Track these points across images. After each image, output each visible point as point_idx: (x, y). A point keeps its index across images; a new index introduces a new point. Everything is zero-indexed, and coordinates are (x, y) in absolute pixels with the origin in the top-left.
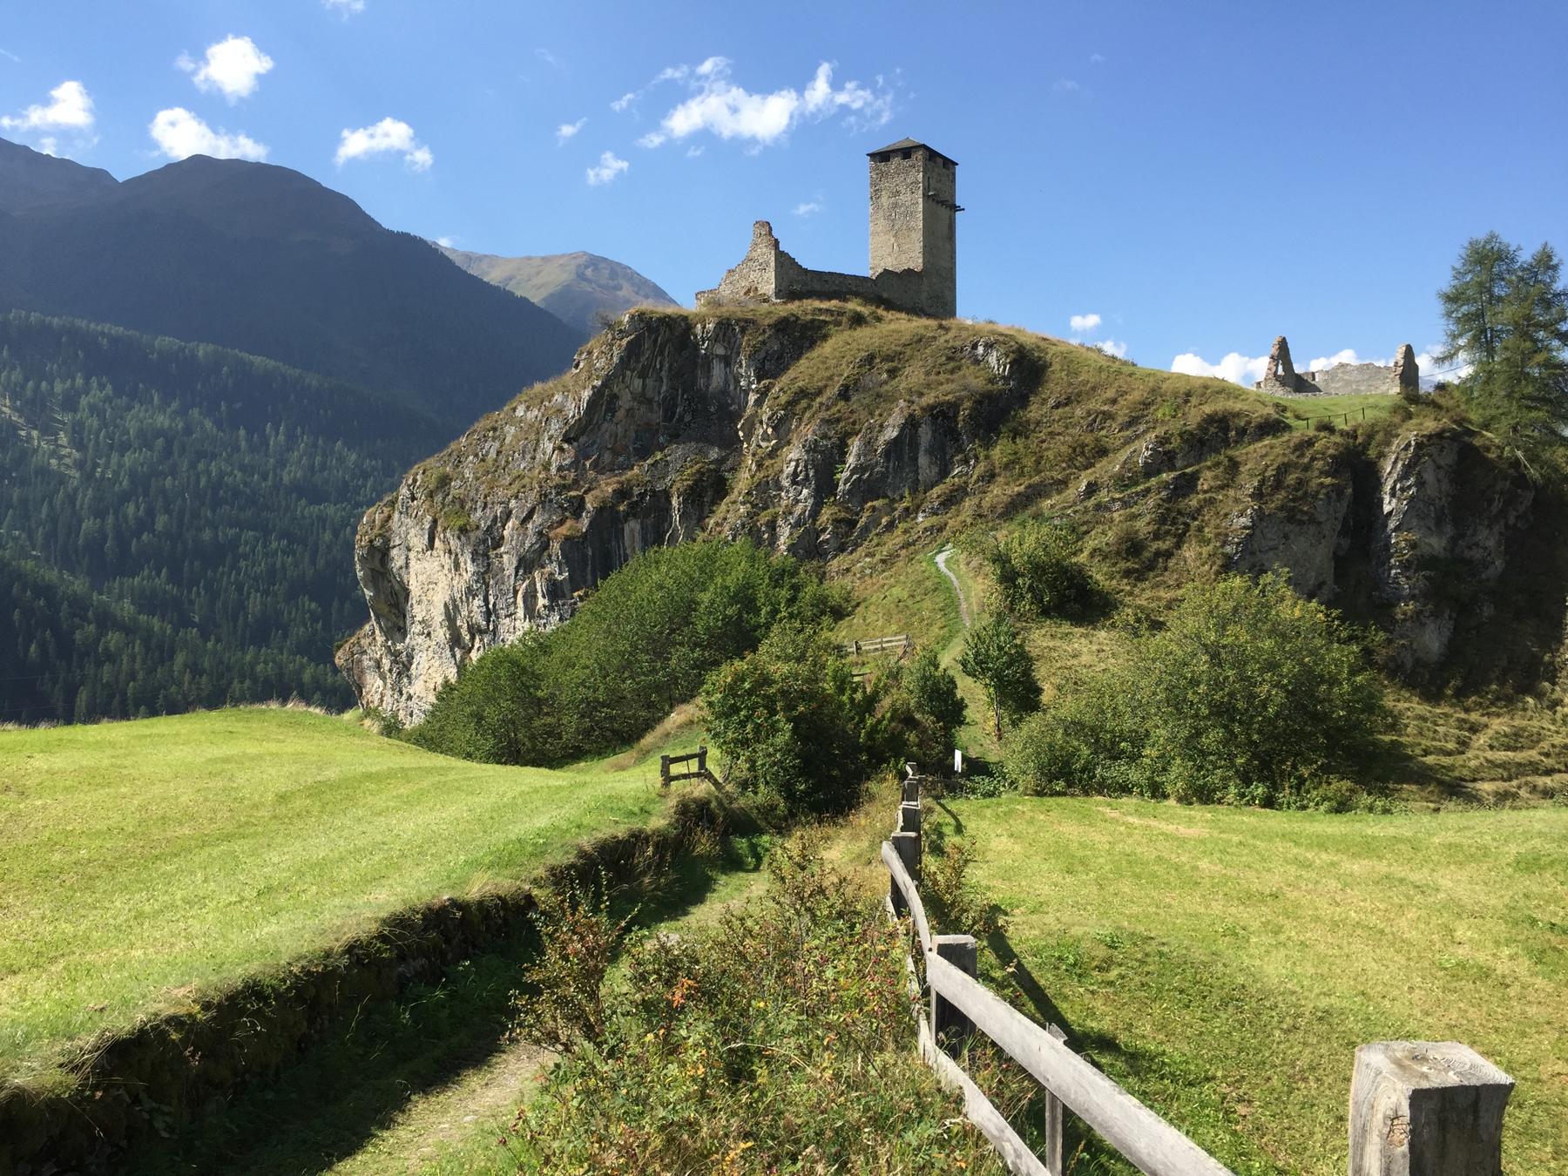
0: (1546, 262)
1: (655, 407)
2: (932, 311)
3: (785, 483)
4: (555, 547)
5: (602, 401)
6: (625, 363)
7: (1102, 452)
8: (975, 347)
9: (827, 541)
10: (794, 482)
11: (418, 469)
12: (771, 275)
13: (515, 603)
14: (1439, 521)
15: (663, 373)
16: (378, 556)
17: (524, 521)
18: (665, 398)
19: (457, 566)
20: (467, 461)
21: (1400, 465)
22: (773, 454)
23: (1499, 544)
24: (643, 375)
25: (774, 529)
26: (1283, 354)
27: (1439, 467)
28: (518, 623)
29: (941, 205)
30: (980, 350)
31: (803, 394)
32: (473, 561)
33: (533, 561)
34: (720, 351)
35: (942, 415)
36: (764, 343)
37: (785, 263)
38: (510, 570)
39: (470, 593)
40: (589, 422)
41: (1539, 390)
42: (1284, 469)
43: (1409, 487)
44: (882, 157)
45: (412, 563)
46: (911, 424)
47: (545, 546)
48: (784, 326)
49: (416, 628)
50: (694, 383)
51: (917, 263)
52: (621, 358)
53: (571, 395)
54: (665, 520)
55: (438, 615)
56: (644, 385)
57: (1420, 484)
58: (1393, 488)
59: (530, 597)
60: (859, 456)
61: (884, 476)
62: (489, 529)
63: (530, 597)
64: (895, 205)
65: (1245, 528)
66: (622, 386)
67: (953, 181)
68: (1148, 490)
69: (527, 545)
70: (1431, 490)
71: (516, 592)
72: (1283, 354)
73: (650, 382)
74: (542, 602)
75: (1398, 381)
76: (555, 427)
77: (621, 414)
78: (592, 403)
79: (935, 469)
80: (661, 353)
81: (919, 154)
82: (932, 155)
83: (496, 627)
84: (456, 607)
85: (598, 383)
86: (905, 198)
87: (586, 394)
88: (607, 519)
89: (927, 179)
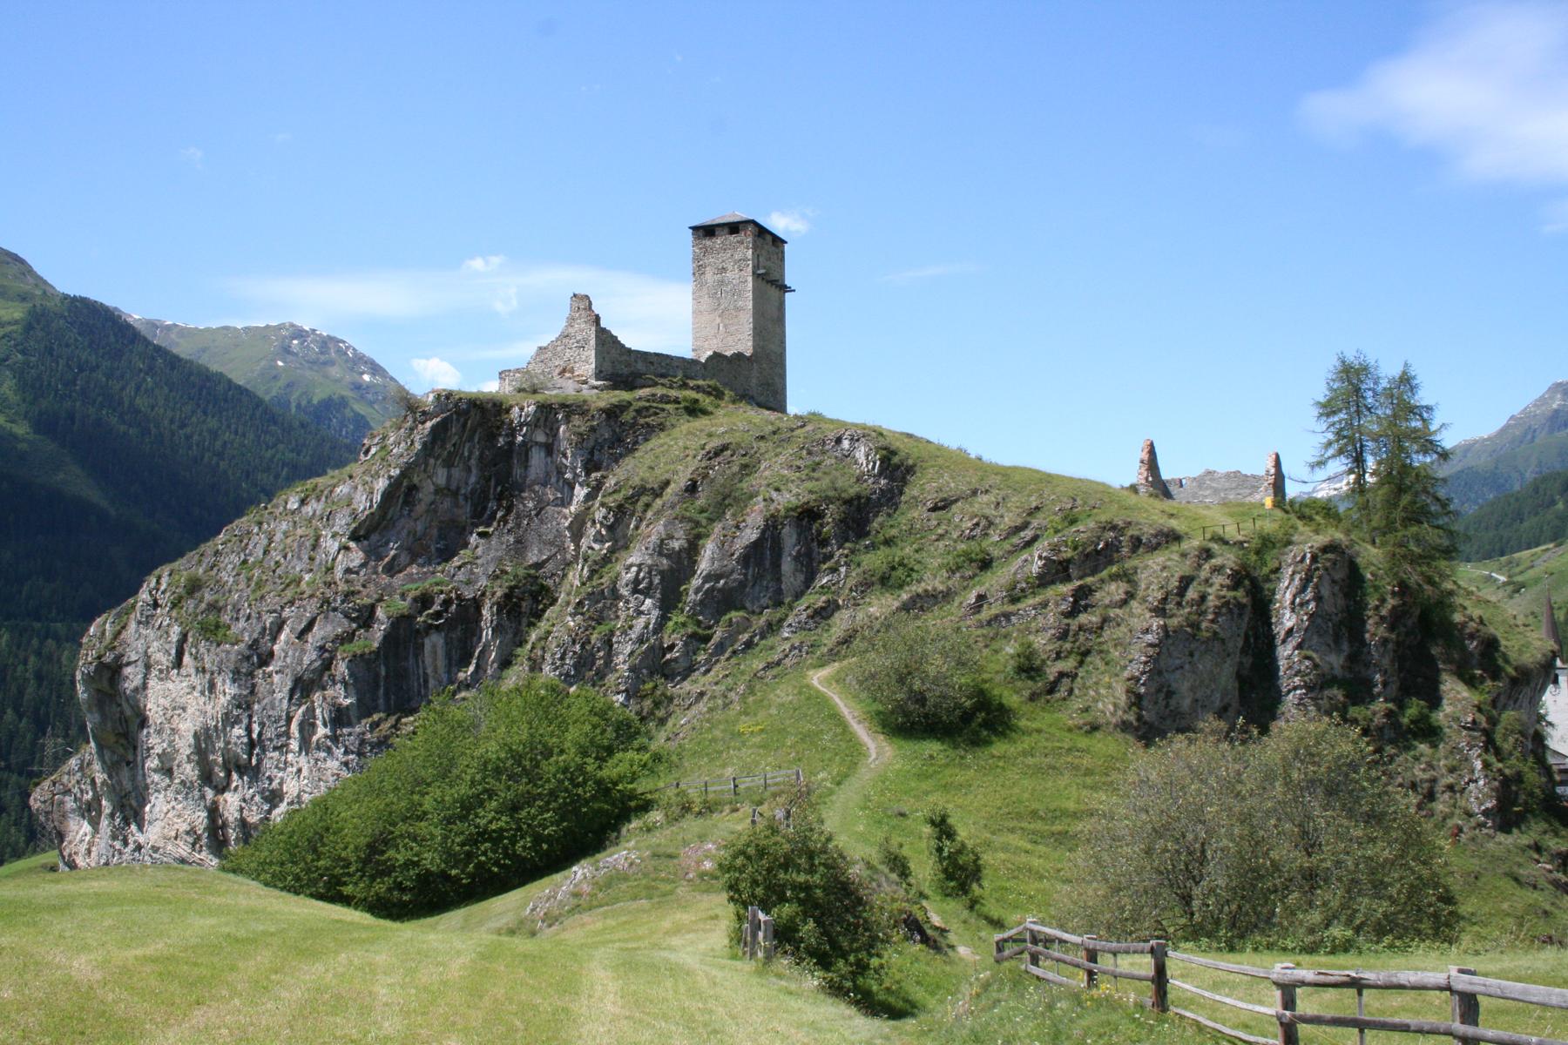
0: (1406, 380)
2: (762, 399)
3: (624, 592)
4: (341, 668)
5: (401, 493)
6: (430, 447)
7: (986, 564)
8: (839, 441)
9: (675, 660)
10: (635, 591)
11: (165, 571)
12: (590, 354)
13: (287, 734)
14: (1337, 639)
15: (473, 462)
16: (107, 674)
17: (302, 635)
18: (473, 492)
19: (212, 686)
20: (225, 559)
21: (1297, 577)
22: (606, 560)
23: (1392, 661)
24: (449, 464)
25: (611, 646)
26: (1152, 464)
27: (1334, 581)
28: (290, 756)
30: (846, 444)
32: (234, 681)
33: (312, 681)
34: (540, 437)
35: (808, 515)
37: (606, 341)
38: (282, 695)
39: (229, 720)
40: (383, 517)
42: (1186, 582)
43: (1308, 602)
44: (706, 232)
45: (151, 683)
46: (772, 527)
47: (327, 665)
48: (612, 413)
49: (153, 763)
50: (509, 474)
51: (746, 346)
52: (425, 445)
53: (360, 489)
54: (473, 635)
55: (185, 746)
56: (449, 477)
57: (1318, 598)
58: (1293, 603)
59: (307, 727)
60: (713, 560)
61: (742, 584)
62: (254, 645)
63: (307, 727)
64: (721, 283)
65: (1151, 645)
66: (423, 476)
68: (1045, 605)
69: (306, 661)
70: (1328, 607)
71: (289, 719)
72: (1152, 464)
73: (457, 473)
74: (322, 731)
75: (1271, 491)
76: (342, 522)
77: (420, 508)
78: (388, 495)
79: (801, 577)
80: (471, 439)
82: (762, 232)
83: (260, 761)
84: (208, 737)
85: (395, 472)
86: (732, 275)
87: (381, 484)
88: (403, 635)
89: (756, 256)
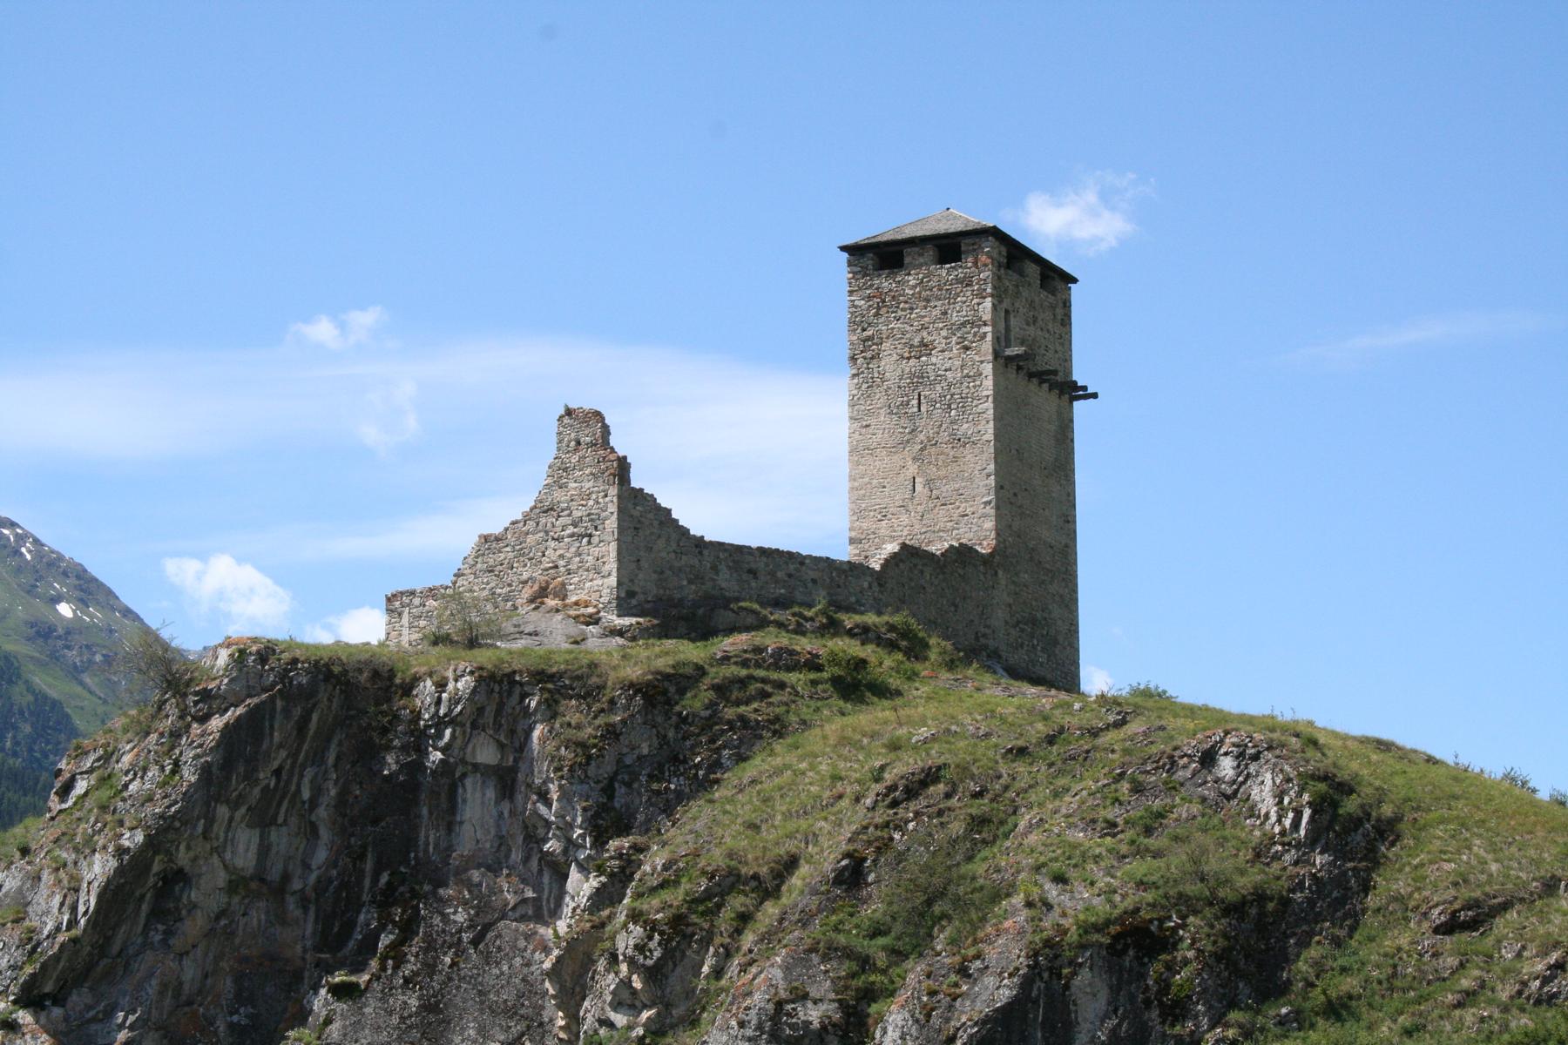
1: (291, 903)
8: (1208, 759)
12: (607, 551)
15: (322, 813)
18: (321, 886)
24: (263, 819)
29: (1040, 384)
30: (1226, 766)
31: (728, 881)
34: (486, 753)
36: (611, 733)
37: (644, 520)
40: (102, 949)
41: (766, 992)
44: (879, 258)
48: (657, 694)
50: (410, 842)
51: (978, 528)
52: (206, 772)
56: (264, 850)
64: (918, 379)
67: (1066, 321)
77: (193, 927)
78: (114, 895)
80: (317, 757)
81: (988, 246)
82: (1014, 255)
85: (133, 839)
87: (99, 868)
89: (1003, 314)
